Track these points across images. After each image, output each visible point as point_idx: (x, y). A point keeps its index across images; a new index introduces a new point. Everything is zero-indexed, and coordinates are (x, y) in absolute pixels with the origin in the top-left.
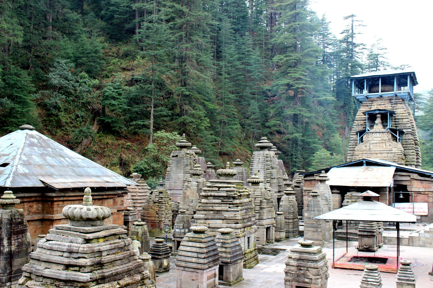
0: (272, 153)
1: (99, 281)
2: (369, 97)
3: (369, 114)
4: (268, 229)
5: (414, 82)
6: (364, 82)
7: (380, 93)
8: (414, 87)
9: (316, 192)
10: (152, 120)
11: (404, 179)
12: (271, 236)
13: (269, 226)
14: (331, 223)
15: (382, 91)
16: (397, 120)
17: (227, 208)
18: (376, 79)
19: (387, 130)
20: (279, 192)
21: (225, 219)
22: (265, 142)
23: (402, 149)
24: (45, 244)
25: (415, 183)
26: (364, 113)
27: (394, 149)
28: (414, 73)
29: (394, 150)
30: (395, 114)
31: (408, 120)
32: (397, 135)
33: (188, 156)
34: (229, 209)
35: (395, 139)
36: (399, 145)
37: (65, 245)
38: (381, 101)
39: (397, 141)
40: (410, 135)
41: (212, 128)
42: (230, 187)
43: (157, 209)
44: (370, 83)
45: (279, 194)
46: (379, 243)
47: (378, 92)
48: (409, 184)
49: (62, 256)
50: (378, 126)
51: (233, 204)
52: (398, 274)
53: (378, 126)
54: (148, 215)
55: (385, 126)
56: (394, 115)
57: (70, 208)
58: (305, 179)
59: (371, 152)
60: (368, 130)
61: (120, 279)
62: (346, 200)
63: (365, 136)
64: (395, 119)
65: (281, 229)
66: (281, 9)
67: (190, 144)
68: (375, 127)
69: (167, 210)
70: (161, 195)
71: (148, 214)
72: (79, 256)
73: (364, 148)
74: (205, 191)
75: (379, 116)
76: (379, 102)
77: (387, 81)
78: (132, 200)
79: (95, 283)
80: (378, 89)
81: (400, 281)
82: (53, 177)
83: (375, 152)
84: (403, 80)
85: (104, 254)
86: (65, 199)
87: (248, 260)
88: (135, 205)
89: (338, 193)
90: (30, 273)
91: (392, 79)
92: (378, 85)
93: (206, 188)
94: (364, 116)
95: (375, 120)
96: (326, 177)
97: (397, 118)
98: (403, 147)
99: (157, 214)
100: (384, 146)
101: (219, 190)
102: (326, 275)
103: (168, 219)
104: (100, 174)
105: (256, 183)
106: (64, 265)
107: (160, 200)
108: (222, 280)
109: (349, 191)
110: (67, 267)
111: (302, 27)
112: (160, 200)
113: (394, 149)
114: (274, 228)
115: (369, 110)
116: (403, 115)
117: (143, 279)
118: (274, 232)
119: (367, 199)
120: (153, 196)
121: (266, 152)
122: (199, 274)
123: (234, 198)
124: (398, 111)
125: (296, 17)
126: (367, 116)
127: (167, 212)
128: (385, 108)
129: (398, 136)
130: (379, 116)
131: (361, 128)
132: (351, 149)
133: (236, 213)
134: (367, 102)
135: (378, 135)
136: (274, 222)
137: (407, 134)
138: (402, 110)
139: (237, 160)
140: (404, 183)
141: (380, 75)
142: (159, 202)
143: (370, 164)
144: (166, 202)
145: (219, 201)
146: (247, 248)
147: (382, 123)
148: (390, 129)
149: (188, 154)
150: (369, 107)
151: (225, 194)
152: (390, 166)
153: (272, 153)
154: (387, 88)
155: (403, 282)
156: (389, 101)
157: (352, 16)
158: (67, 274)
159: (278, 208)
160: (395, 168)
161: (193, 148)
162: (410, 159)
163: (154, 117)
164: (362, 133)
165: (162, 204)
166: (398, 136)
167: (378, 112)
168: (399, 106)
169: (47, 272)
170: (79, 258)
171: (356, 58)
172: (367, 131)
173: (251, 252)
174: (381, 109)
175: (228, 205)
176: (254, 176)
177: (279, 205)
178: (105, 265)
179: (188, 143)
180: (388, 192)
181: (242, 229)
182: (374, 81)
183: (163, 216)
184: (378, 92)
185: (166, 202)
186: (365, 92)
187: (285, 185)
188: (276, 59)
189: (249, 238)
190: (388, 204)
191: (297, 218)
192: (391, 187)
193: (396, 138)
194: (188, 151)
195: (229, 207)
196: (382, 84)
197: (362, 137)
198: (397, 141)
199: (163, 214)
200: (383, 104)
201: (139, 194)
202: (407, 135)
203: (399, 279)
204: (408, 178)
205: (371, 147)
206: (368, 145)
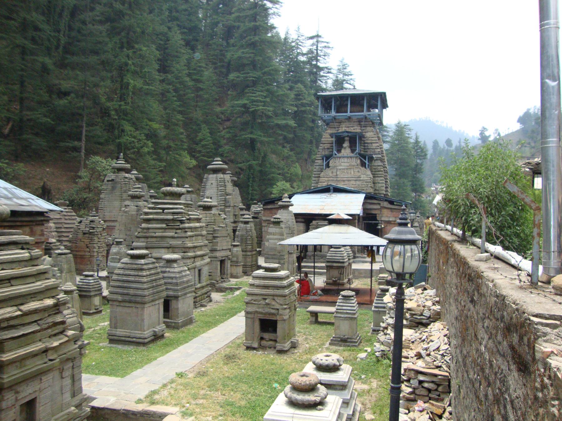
0: (227, 177)
2: (337, 118)
3: (336, 137)
4: (222, 262)
6: (332, 102)
7: (349, 114)
8: (384, 110)
9: (279, 218)
10: (84, 142)
11: (374, 207)
12: (226, 271)
13: (223, 258)
14: (296, 247)
15: (351, 112)
16: (366, 145)
17: (173, 234)
19: (356, 154)
20: (235, 222)
21: (170, 248)
22: (218, 163)
23: (371, 176)
25: (385, 212)
26: (331, 135)
27: (362, 176)
29: (363, 177)
30: (364, 137)
31: (377, 144)
32: (365, 160)
33: (127, 180)
34: (176, 235)
35: (363, 165)
36: (369, 172)
39: (365, 168)
40: (379, 161)
41: (155, 152)
42: (177, 209)
43: (87, 241)
44: (338, 103)
45: (234, 225)
46: (348, 276)
47: (347, 112)
48: (379, 213)
50: (346, 151)
51: (180, 229)
53: (346, 151)
54: (77, 249)
55: (353, 151)
56: (363, 139)
58: (265, 207)
60: (336, 155)
64: (365, 143)
65: (237, 262)
66: (239, 21)
67: (128, 166)
68: (343, 151)
71: (76, 247)
73: (331, 175)
74: (146, 214)
75: (347, 138)
76: (347, 124)
78: (56, 233)
81: (377, 309)
84: (373, 102)
87: (198, 297)
88: (61, 239)
92: (347, 105)
93: (147, 210)
94: (331, 139)
95: (343, 143)
96: (290, 202)
97: (366, 141)
98: (372, 174)
99: (88, 247)
100: (352, 173)
101: (163, 212)
103: (102, 254)
105: (207, 208)
108: (168, 318)
109: (315, 220)
111: (263, 41)
113: (362, 176)
114: (229, 261)
115: (336, 132)
116: (373, 139)
118: (229, 266)
121: (221, 175)
122: (140, 309)
123: (182, 222)
124: (368, 135)
125: (255, 30)
126: (334, 139)
127: (99, 245)
128: (354, 131)
129: (367, 162)
131: (327, 153)
132: (316, 176)
133: (183, 240)
134: (335, 124)
135: (346, 160)
137: (377, 160)
138: (372, 133)
140: (373, 212)
142: (90, 233)
143: (338, 190)
144: (99, 233)
145: (164, 226)
146: (197, 282)
147: (351, 147)
148: (360, 154)
150: (337, 129)
151: (170, 217)
153: (227, 177)
155: (380, 309)
157: (318, 36)
161: (133, 172)
162: (379, 187)
163: (86, 139)
164: (328, 158)
165: (94, 235)
166: (367, 162)
167: (347, 134)
168: (369, 129)
171: (319, 82)
172: (334, 156)
173: (203, 287)
174: (350, 131)
175: (174, 231)
176: (206, 200)
177: (234, 235)
180: (357, 221)
181: (193, 260)
183: (95, 250)
184: (347, 112)
185: (99, 233)
186: (333, 113)
188: (232, 76)
189: (200, 271)
191: (256, 250)
193: (365, 163)
194: (127, 175)
195: (176, 233)
199: (94, 248)
201: (66, 226)
202: (376, 161)
204: (378, 207)
205: (338, 173)
206: (335, 171)
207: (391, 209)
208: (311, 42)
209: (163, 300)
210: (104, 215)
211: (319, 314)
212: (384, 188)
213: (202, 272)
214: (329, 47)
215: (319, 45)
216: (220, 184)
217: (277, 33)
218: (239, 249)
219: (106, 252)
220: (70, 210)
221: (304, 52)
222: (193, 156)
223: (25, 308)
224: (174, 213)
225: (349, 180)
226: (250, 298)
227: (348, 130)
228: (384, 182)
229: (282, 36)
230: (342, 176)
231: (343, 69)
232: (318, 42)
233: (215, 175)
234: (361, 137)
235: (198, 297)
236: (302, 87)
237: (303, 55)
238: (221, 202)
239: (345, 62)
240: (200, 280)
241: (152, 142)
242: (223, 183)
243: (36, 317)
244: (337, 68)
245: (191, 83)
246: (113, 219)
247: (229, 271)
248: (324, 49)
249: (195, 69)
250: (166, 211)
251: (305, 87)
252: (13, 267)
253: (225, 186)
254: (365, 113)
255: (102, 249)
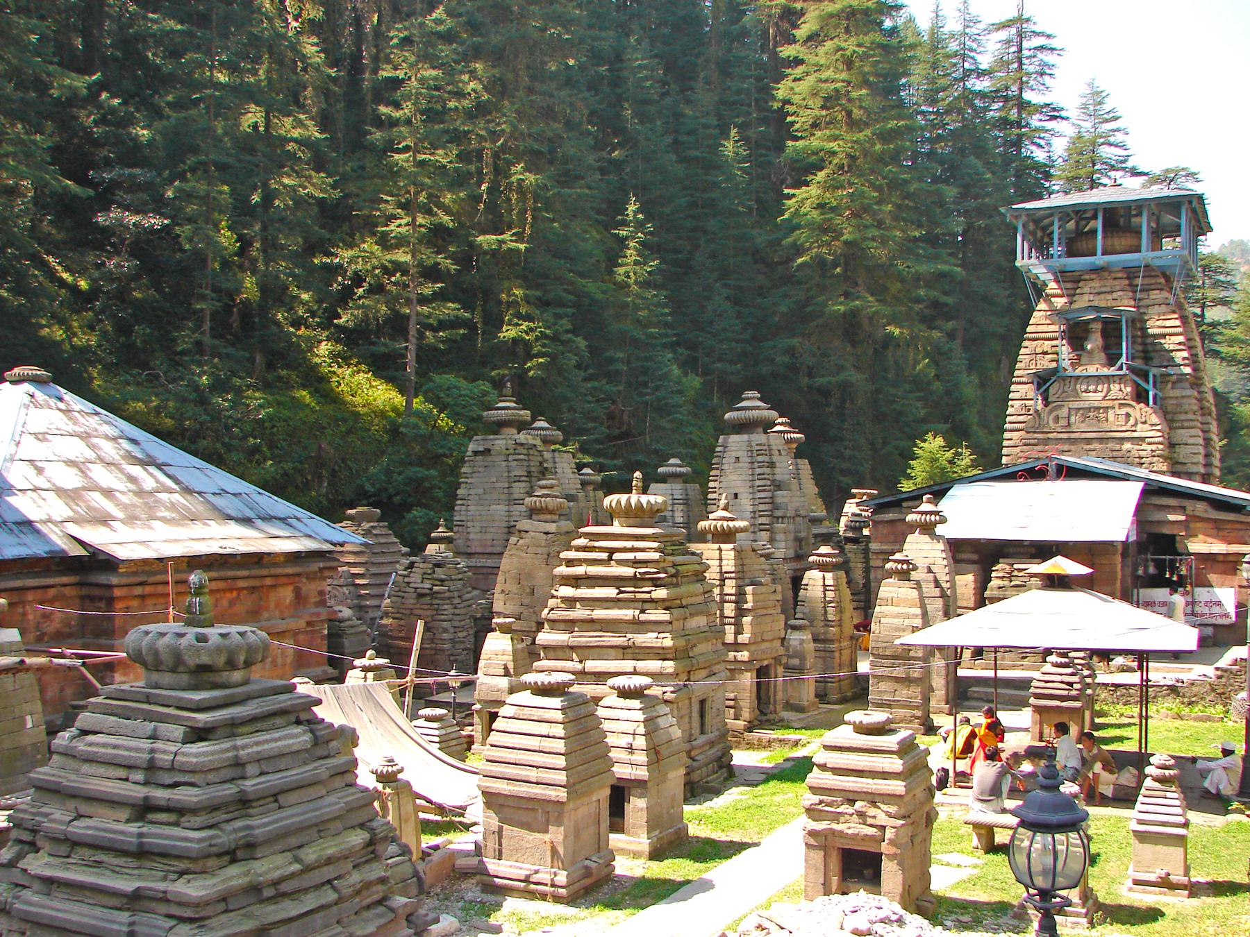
1: (239, 854)
5: (1201, 225)
7: (1099, 260)
13: (766, 663)
18: (1088, 215)
22: (752, 405)
24: (75, 743)
28: (1200, 198)
32: (1148, 382)
33: (520, 450)
37: (136, 747)
38: (1102, 283)
39: (1147, 405)
49: (127, 780)
52: (1138, 806)
55: (1112, 360)
57: (147, 633)
59: (1073, 436)
61: (301, 847)
62: (994, 583)
63: (1056, 385)
69: (458, 618)
70: (440, 574)
72: (176, 779)
77: (1122, 221)
78: (351, 588)
79: (227, 858)
80: (1095, 248)
82: (109, 526)
83: (1084, 436)
85: (251, 770)
86: (148, 589)
87: (699, 768)
89: (974, 562)
90: (34, 832)
91: (1136, 215)
95: (1086, 339)
96: (937, 513)
101: (610, 559)
102: (928, 814)
104: (250, 514)
106: (133, 805)
107: (435, 588)
110: (144, 810)
112: (435, 588)
114: (780, 670)
117: (371, 842)
119: (1056, 582)
120: (415, 578)
130: (1098, 326)
136: (782, 651)
139: (672, 461)
140: (1166, 530)
141: (1098, 204)
142: (433, 594)
144: (456, 594)
149: (522, 444)
151: (628, 571)
152: (1125, 478)
154: (1117, 242)
156: (1127, 282)
158: (141, 835)
159: (795, 609)
160: (1140, 485)
166: (1150, 387)
169: (80, 828)
170: (175, 785)
174: (1103, 304)
178: (254, 804)
179: (522, 412)
180: (1119, 558)
182: (1082, 219)
183: (445, 635)
185: (456, 594)
187: (816, 536)
190: (1118, 593)
192: (1130, 540)
194: (523, 437)
196: (1104, 232)
197: (1047, 390)
198: (1147, 405)
200: (1108, 289)
203: (1140, 822)
205: (1073, 419)
207: (1216, 521)
208: (1003, 35)
209: (608, 791)
210: (468, 539)
211: (996, 829)
212: (1201, 459)
213: (708, 705)
214: (1052, 49)
215: (1026, 44)
216: (760, 458)
217: (911, 20)
218: (806, 636)
219: (472, 640)
220: (385, 531)
221: (984, 66)
222: (689, 365)
223: (310, 855)
224: (636, 563)
225: (1101, 440)
226: (816, 799)
227: (1099, 302)
228: (1201, 441)
229: (924, 24)
230: (1083, 427)
231: (1095, 102)
232: (1021, 36)
233: (745, 437)
234: (1138, 323)
235: (699, 768)
236: (979, 164)
237: (981, 74)
238: (762, 507)
239: (1102, 85)
240: (702, 725)
241: (585, 338)
242: (766, 459)
243: (328, 872)
244: (1079, 101)
245: (679, 170)
246: (489, 550)
247: (780, 696)
248: (1040, 55)
249: (691, 133)
250: (616, 556)
251: (987, 164)
252: (282, 767)
253: (772, 465)
254: (1145, 255)
255: (465, 634)
